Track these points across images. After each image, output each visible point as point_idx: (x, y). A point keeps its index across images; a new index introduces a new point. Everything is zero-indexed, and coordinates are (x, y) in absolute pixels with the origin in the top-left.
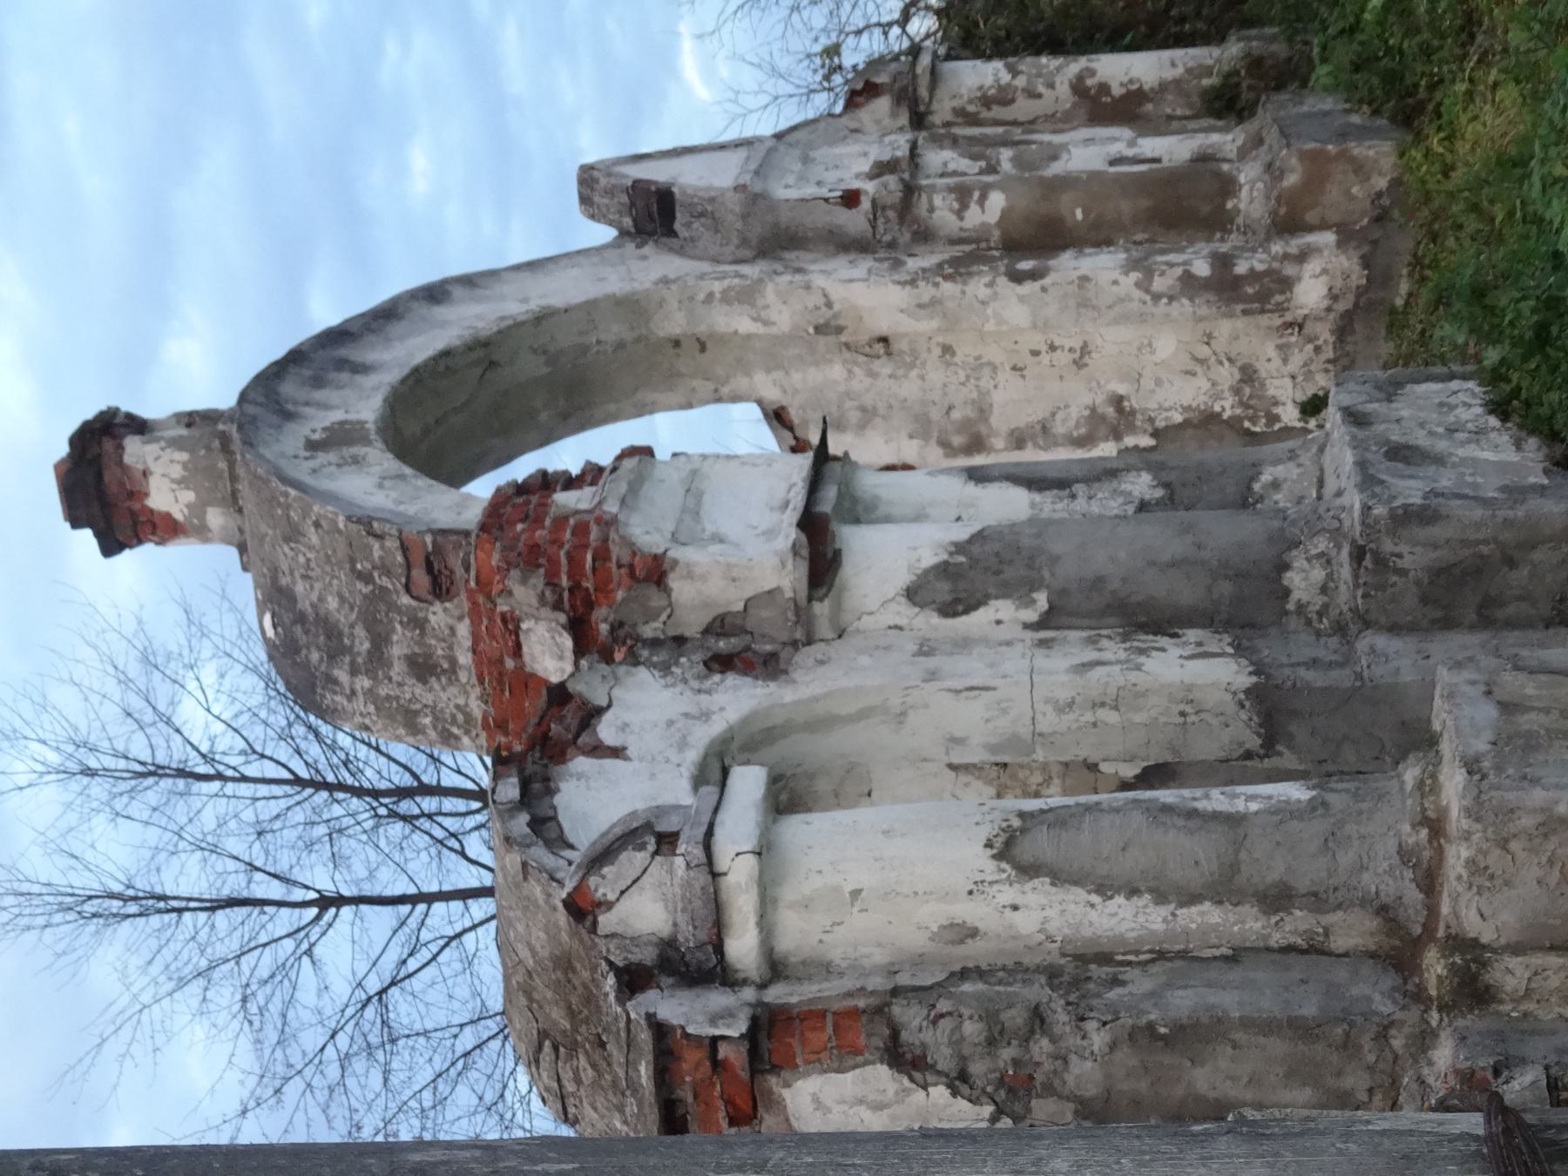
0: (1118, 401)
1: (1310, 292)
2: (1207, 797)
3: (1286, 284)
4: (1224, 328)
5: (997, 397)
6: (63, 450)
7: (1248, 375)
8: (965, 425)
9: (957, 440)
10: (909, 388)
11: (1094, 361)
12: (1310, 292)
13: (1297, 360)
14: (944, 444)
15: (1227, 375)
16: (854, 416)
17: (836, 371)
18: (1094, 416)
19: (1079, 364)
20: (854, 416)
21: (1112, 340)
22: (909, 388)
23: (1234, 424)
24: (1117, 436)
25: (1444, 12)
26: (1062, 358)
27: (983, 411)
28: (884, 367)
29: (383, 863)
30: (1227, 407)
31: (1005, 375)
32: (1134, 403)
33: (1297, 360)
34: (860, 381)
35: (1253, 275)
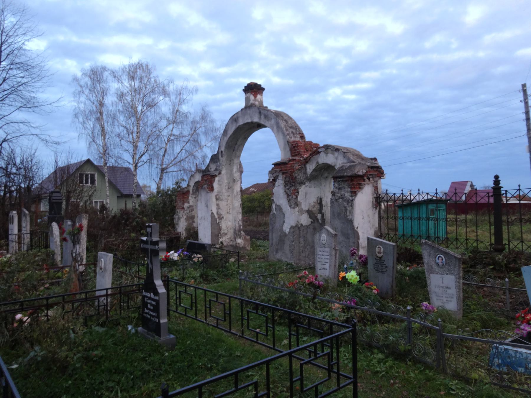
0: (223, 218)
1: (239, 241)
2: (27, 238)
3: (240, 238)
4: (232, 231)
5: (223, 202)
6: (314, 142)
7: (226, 234)
8: (220, 198)
9: (218, 197)
10: (224, 191)
11: (228, 215)
12: (239, 241)
13: (227, 240)
14: (217, 195)
15: (226, 232)
16: (220, 183)
17: (226, 181)
18: (221, 215)
19: (228, 213)
20: (220, 183)
21: (230, 217)
22: (224, 191)
23: (220, 233)
24: (218, 218)
25: (93, 262)
26: (228, 210)
27: (222, 200)
28: (227, 187)
29: (498, 246)
30: (222, 232)
31: (226, 203)
32: (223, 220)
33: (227, 240)
34: (225, 184)
35: (241, 234)
